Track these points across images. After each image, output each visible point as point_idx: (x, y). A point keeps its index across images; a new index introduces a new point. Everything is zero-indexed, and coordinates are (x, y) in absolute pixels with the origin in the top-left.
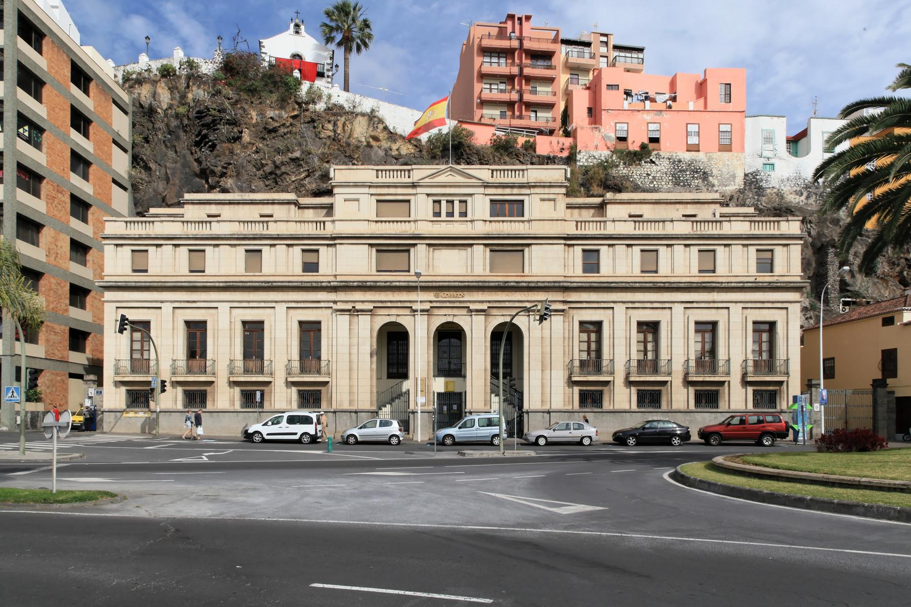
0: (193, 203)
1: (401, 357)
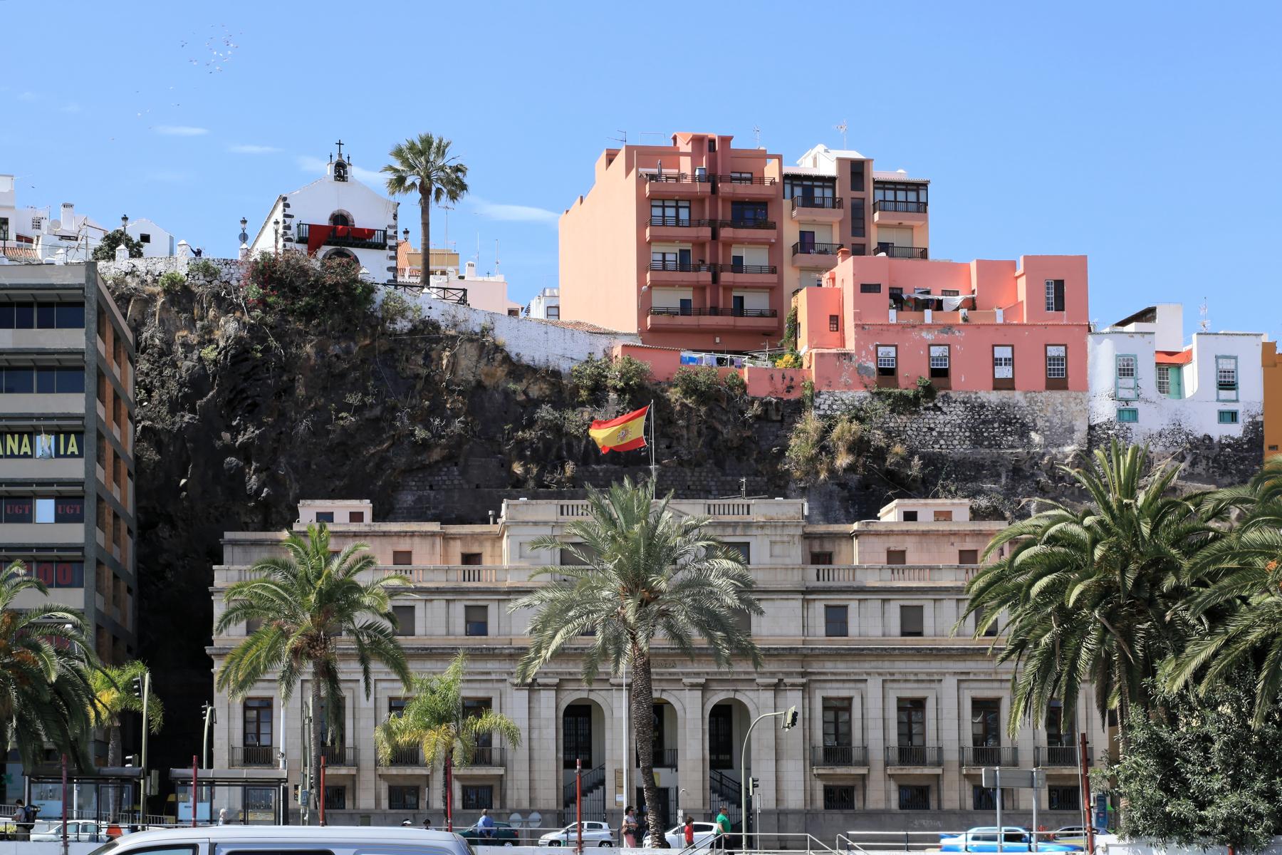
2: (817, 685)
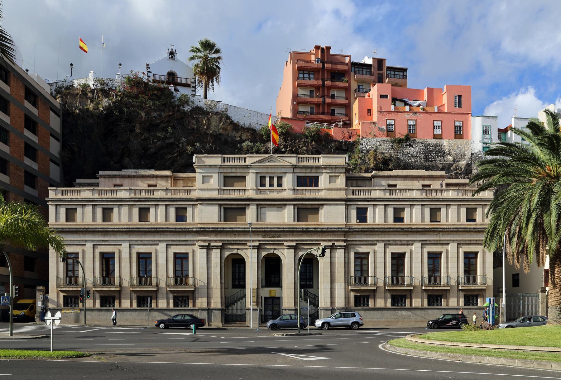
0: (104, 177)
1: (241, 274)
2: (352, 246)
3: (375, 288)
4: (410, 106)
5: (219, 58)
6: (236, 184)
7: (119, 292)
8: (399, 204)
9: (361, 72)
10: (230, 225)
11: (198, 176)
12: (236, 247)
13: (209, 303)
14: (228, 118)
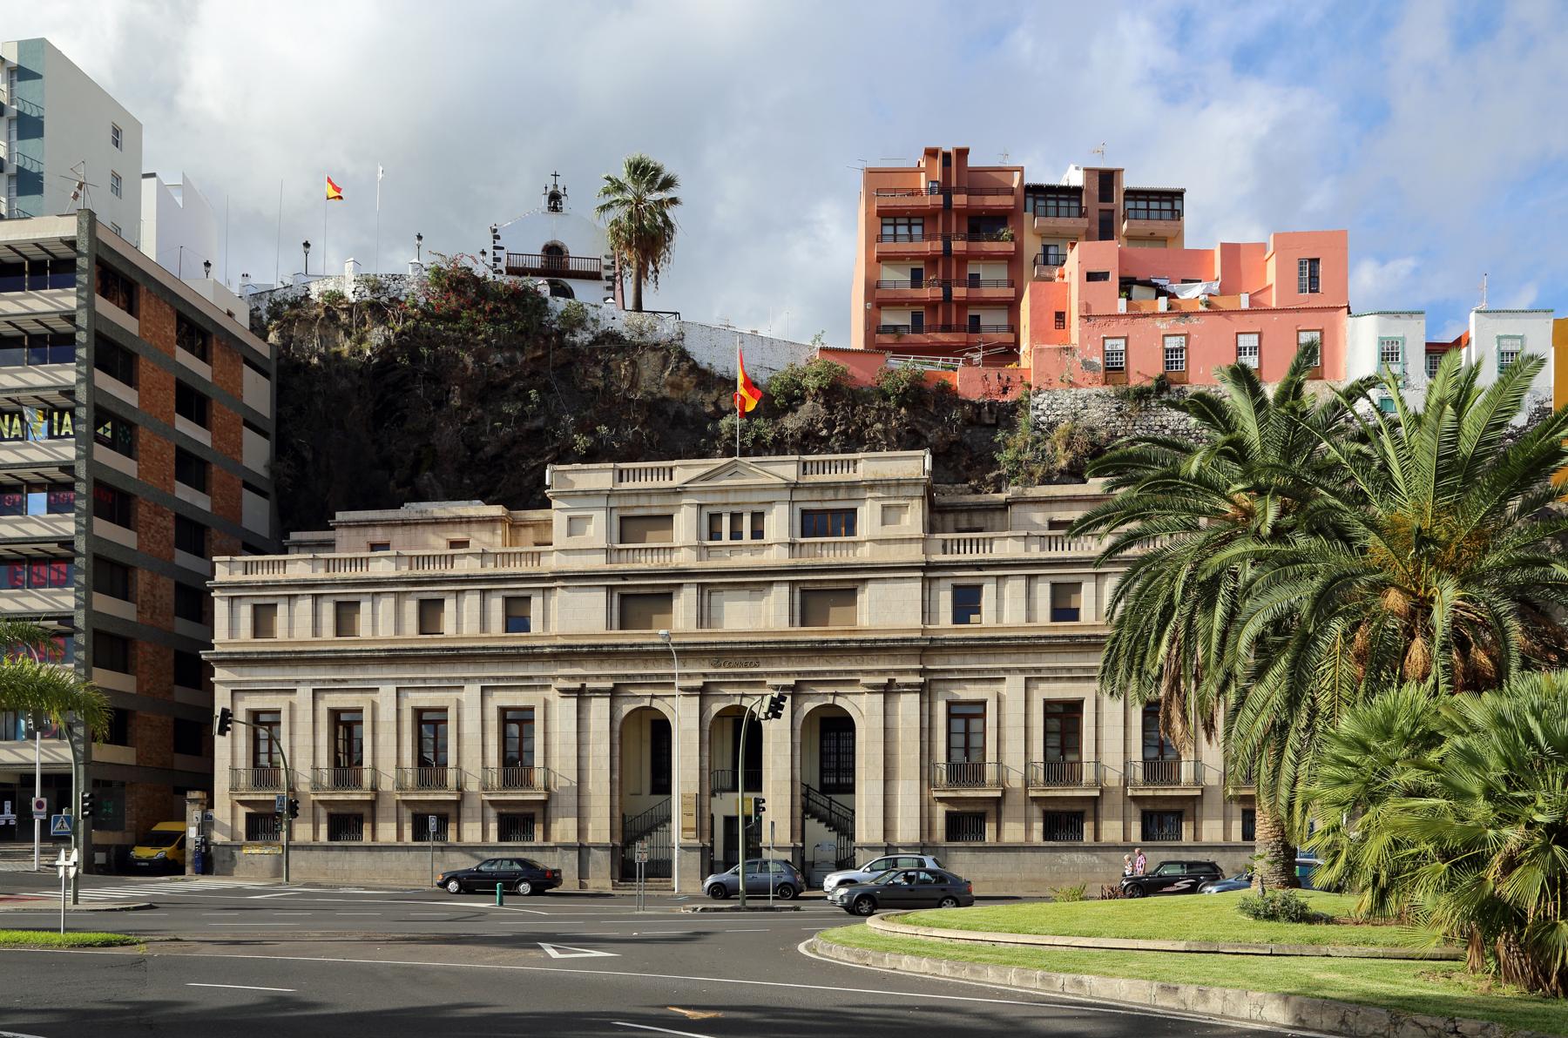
0: (348, 525)
2: (941, 685)
3: (1097, 793)
4: (1172, 296)
5: (674, 201)
6: (650, 534)
7: (372, 804)
8: (1065, 575)
9: (1052, 211)
10: (634, 637)
11: (558, 515)
12: (649, 692)
13: (581, 831)
14: (684, 355)
